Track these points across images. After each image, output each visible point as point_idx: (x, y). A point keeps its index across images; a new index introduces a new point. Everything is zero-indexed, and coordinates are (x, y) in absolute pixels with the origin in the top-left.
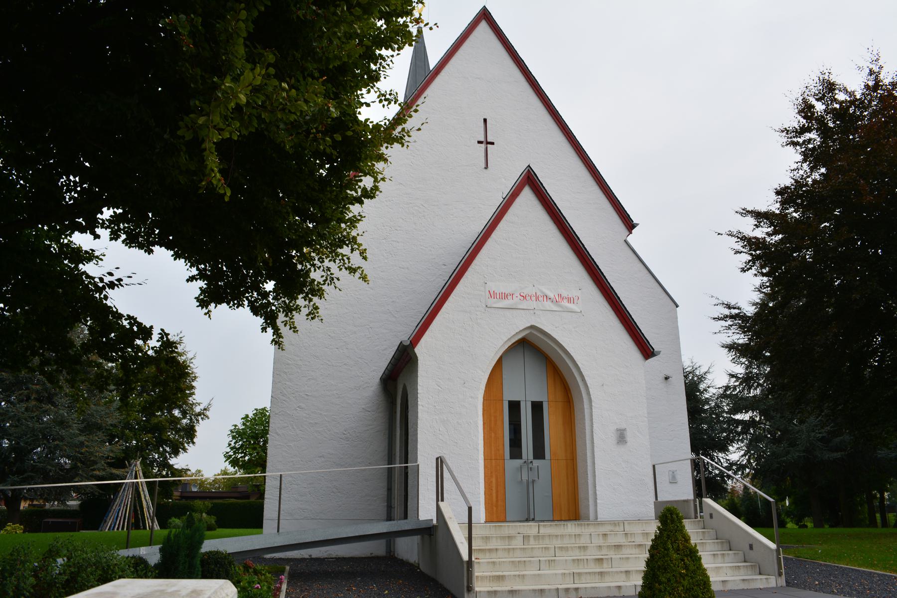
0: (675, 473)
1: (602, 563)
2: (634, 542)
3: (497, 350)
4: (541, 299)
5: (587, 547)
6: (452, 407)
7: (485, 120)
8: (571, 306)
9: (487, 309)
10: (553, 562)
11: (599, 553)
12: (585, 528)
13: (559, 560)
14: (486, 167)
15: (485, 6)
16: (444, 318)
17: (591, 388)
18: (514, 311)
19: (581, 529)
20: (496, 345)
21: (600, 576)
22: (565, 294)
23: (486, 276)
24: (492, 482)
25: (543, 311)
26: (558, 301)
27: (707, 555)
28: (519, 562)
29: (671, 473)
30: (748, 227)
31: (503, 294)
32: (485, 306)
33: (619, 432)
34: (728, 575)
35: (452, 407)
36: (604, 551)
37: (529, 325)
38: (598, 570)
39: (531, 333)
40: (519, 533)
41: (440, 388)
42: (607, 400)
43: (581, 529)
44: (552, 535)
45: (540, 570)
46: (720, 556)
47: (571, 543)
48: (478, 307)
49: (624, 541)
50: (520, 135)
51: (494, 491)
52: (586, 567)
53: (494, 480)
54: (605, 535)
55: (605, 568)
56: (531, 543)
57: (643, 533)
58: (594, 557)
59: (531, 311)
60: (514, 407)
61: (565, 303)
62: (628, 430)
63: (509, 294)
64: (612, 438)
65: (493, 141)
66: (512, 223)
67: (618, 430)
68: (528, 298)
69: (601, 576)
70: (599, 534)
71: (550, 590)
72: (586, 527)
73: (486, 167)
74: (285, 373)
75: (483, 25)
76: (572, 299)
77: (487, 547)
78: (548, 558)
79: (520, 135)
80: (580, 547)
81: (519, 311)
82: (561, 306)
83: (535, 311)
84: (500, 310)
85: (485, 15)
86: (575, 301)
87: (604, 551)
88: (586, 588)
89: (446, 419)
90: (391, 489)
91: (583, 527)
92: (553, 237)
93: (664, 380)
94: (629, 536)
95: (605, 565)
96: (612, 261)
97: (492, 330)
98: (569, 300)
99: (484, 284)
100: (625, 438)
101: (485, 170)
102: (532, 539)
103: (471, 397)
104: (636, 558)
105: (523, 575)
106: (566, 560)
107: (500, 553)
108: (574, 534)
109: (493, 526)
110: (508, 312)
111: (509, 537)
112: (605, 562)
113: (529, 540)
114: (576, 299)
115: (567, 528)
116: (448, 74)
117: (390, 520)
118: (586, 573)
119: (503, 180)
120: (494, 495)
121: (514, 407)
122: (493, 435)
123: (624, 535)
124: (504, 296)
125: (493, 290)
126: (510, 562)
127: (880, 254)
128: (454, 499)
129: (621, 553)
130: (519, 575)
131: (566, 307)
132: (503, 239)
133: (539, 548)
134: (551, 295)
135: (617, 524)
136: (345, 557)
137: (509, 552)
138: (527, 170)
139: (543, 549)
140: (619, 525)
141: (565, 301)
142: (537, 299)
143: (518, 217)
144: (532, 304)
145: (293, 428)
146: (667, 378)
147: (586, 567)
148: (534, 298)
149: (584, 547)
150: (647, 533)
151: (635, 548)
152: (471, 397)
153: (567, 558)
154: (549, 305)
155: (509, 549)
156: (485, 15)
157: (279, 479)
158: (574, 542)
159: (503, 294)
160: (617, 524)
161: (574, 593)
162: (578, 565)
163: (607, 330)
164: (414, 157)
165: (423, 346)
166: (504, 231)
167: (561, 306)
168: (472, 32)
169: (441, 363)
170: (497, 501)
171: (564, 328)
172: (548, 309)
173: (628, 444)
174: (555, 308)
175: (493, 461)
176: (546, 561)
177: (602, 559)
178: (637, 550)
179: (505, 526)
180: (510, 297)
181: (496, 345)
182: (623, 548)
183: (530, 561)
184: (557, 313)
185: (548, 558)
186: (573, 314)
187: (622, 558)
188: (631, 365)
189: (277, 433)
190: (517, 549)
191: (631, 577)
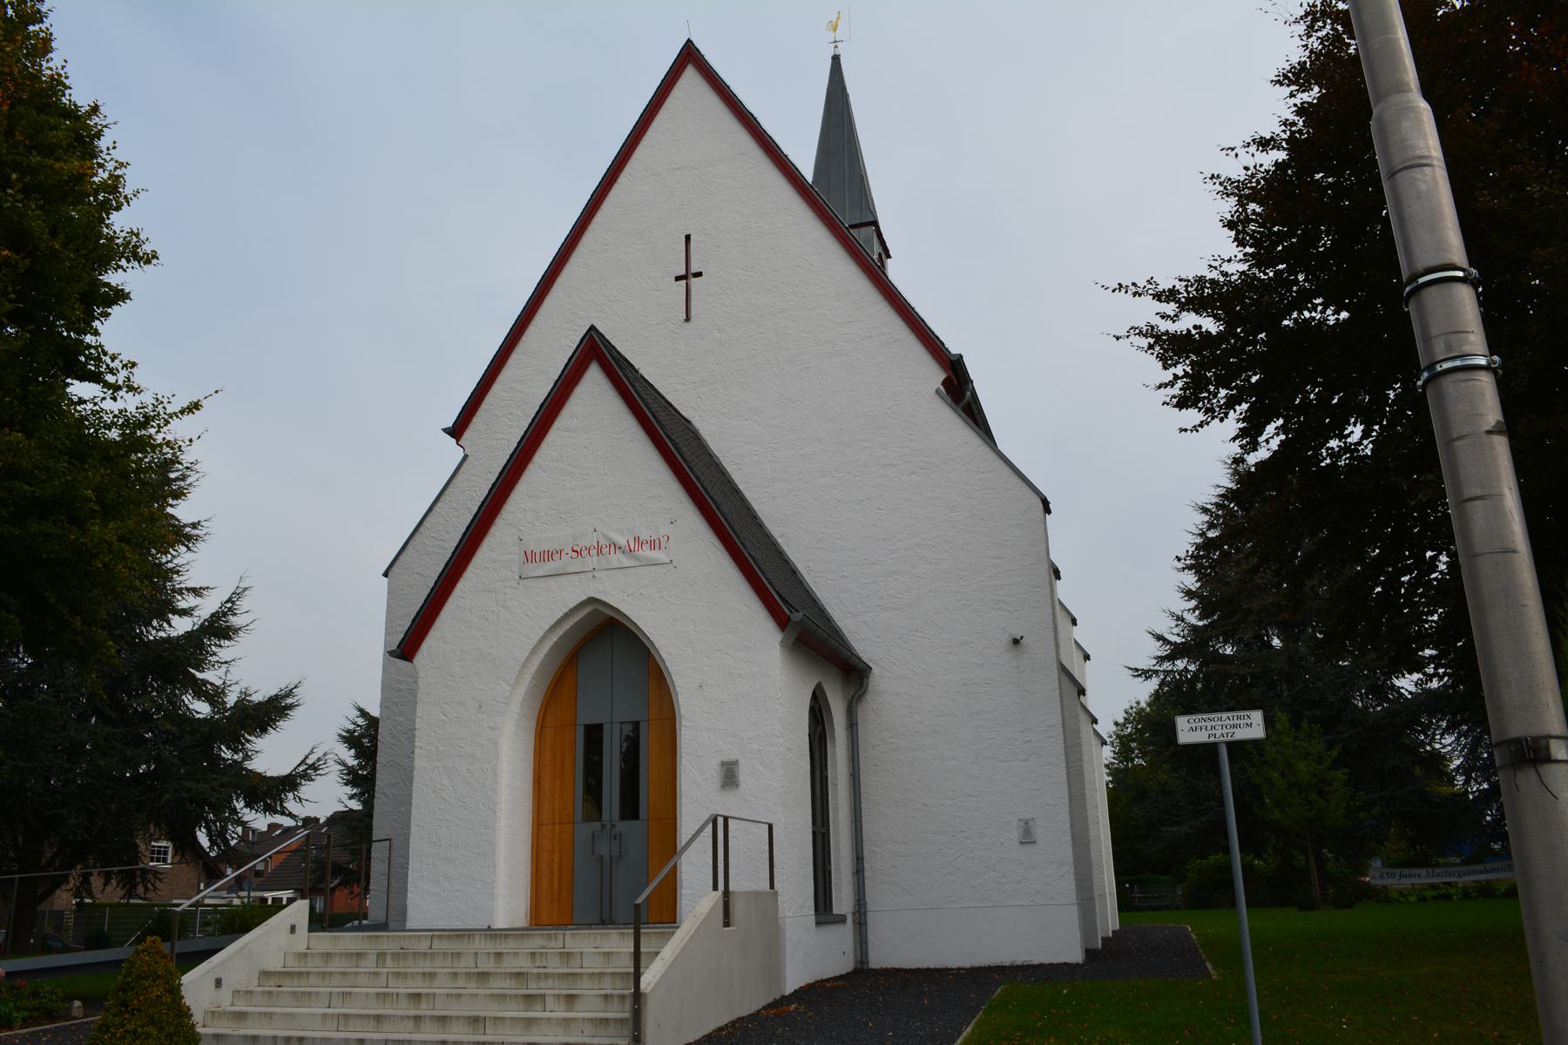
0: (1031, 823)
1: (420, 1002)
2: (544, 967)
3: (531, 647)
4: (605, 550)
5: (435, 973)
6: (462, 747)
7: (688, 238)
8: (657, 555)
9: (522, 582)
10: (348, 996)
11: (453, 985)
12: (469, 942)
13: (357, 993)
14: (688, 319)
15: (689, 40)
16: (458, 606)
17: (681, 694)
18: (563, 579)
19: (495, 943)
20: (531, 639)
21: (375, 1023)
22: (645, 536)
23: (521, 528)
24: (553, 861)
25: (610, 572)
26: (632, 550)
27: (593, 995)
28: (303, 993)
29: (1022, 824)
30: (1148, 312)
31: (546, 553)
32: (517, 577)
33: (725, 767)
34: (586, 1033)
35: (462, 747)
36: (461, 982)
37: (584, 598)
38: (413, 1013)
39: (595, 609)
40: (402, 949)
41: (446, 718)
42: (708, 713)
43: (495, 943)
44: (418, 953)
45: (329, 1007)
46: (616, 1000)
47: (447, 965)
48: (507, 581)
49: (529, 965)
50: (745, 246)
51: (556, 876)
52: (395, 1006)
53: (556, 857)
54: (499, 955)
55: (424, 1010)
56: (387, 966)
57: (561, 953)
58: (446, 991)
59: (590, 574)
60: (594, 735)
61: (646, 552)
63: (555, 552)
64: (714, 776)
65: (700, 270)
66: (568, 431)
67: (723, 764)
68: (585, 553)
69: (378, 1022)
70: (489, 954)
71: (265, 1037)
72: (503, 940)
73: (688, 319)
74: (396, 703)
75: (690, 75)
76: (657, 541)
77: (328, 970)
78: (343, 989)
79: (745, 246)
80: (424, 974)
81: (569, 577)
82: (638, 559)
83: (596, 574)
84: (542, 579)
85: (690, 56)
86: (663, 546)
87: (461, 982)
88: (314, 1038)
89: (451, 765)
90: (858, 859)
91: (498, 941)
92: (632, 440)
93: (1012, 642)
94: (538, 956)
95: (423, 1005)
96: (911, 434)
97: (527, 615)
98: (653, 545)
100: (735, 777)
101: (686, 324)
102: (389, 960)
103: (490, 728)
104: (472, 995)
105: (271, 1014)
106: (367, 994)
107: (313, 980)
108: (451, 951)
109: (367, 936)
110: (551, 581)
111: (357, 954)
112: (424, 999)
113: (385, 961)
115: (473, 941)
116: (630, 177)
117: (1517, 892)
118: (357, 1016)
119: (716, 333)
120: (556, 881)
121: (594, 735)
122: (558, 783)
123: (530, 955)
124: (548, 556)
125: (531, 548)
126: (290, 992)
127: (1344, 315)
128: (457, 890)
129: (488, 986)
130: (265, 1013)
131: (646, 558)
132: (552, 461)
133: (365, 973)
134: (622, 541)
135: (553, 937)
136: (938, 967)
137: (324, 978)
138: (589, 335)
139: (371, 975)
140: (556, 937)
142: (600, 551)
143: (577, 418)
144: (592, 561)
145: (406, 785)
146: (1016, 642)
147: (395, 1006)
148: (594, 552)
149: (430, 974)
150: (568, 953)
151: (511, 979)
152: (490, 728)
153: (369, 990)
154: (617, 559)
155: (324, 973)
156: (690, 56)
157: (387, 861)
158: (450, 965)
159: (546, 553)
160: (553, 937)
161: (297, 1043)
162: (384, 1002)
163: (716, 587)
164: (576, 331)
165: (425, 655)
166: (554, 448)
167: (638, 559)
168: (670, 92)
169: (450, 678)
170: (560, 891)
171: (641, 594)
172: (615, 564)
173: (742, 787)
174: (626, 562)
175: (557, 827)
176: (339, 993)
177: (419, 995)
178: (513, 981)
179: (383, 936)
180: (556, 556)
181: (531, 639)
182: (491, 978)
183: (317, 993)
184: (631, 570)
185: (343, 989)
186: (659, 567)
187: (451, 995)
188: (755, 645)
189: (384, 793)
190: (335, 973)
191: (422, 1025)
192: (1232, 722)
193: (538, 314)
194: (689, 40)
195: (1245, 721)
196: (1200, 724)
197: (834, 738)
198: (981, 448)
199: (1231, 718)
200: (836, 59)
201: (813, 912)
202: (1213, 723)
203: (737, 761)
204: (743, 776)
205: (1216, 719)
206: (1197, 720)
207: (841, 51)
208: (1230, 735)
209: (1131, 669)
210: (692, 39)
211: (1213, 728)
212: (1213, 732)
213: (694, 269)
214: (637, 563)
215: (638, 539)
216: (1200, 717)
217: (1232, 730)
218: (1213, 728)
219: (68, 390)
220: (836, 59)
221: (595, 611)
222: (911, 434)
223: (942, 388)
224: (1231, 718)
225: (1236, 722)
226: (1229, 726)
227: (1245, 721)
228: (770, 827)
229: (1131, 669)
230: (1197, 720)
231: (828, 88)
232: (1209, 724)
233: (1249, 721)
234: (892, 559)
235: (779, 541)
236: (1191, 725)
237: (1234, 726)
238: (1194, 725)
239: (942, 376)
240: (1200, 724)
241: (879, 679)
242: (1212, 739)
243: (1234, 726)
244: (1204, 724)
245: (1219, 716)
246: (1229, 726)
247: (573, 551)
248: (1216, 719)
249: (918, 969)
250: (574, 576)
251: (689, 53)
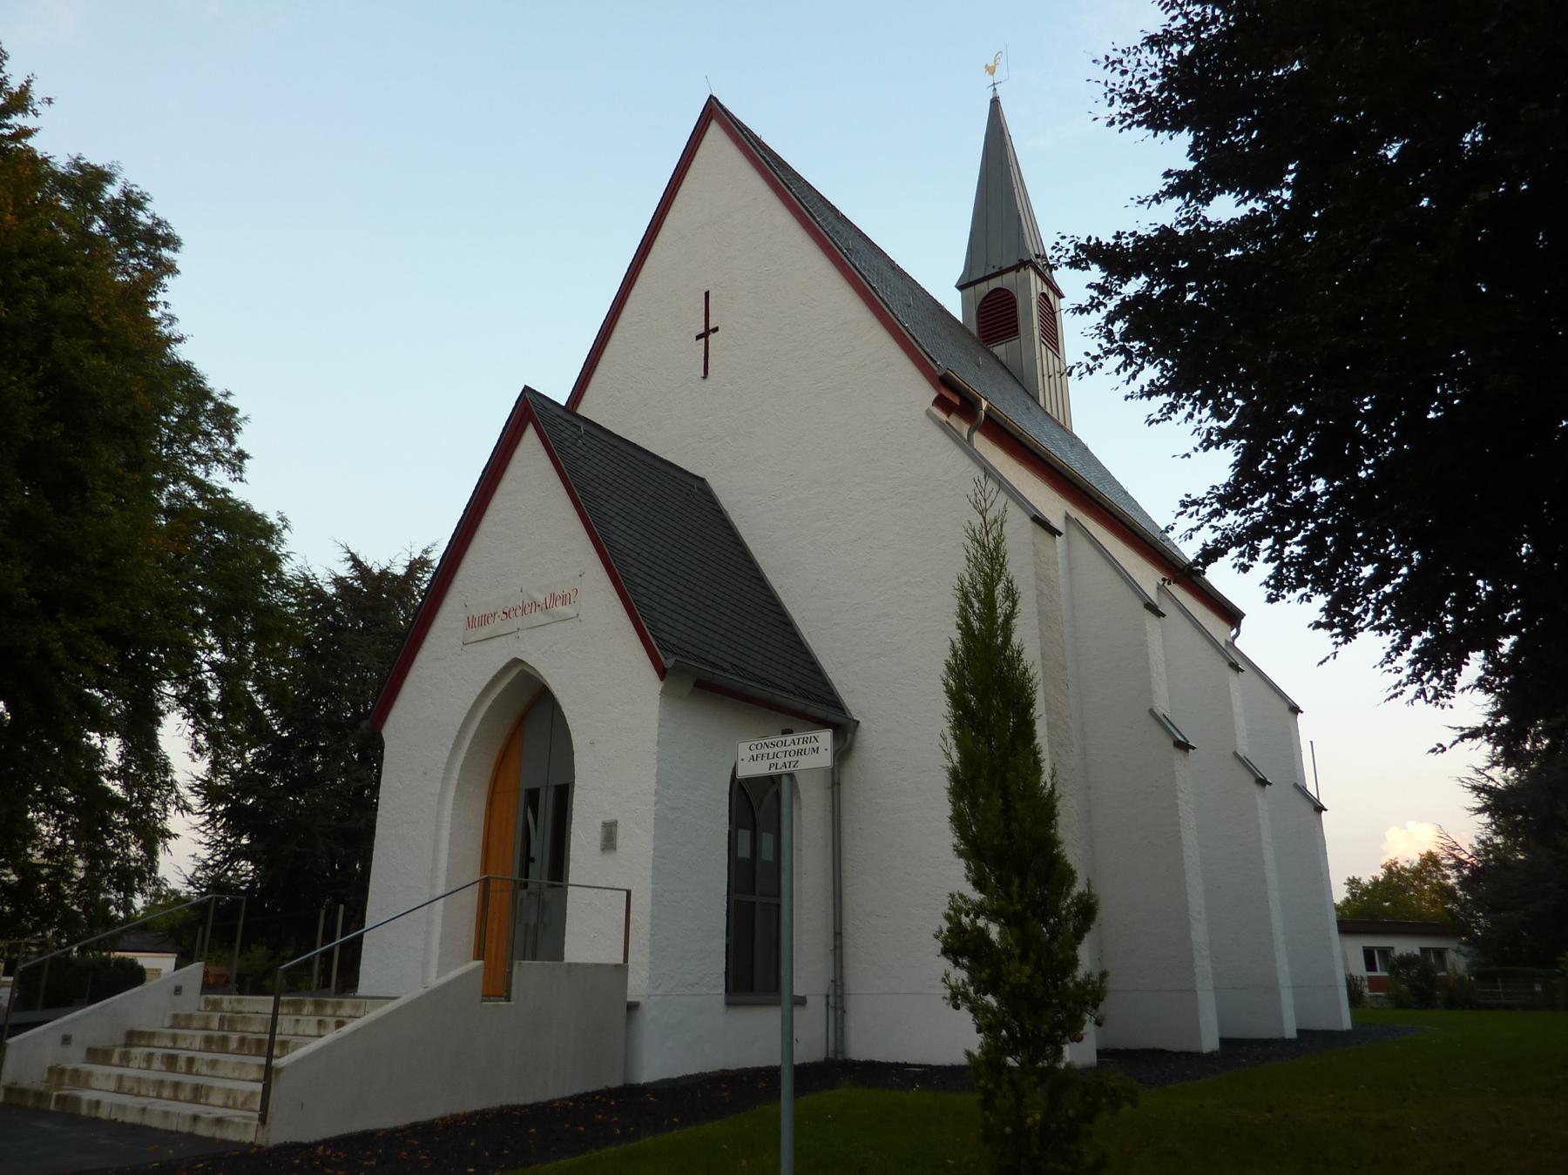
4: (528, 610)
7: (707, 294)
9: (465, 648)
18: (494, 642)
61: (560, 609)
62: (619, 819)
67: (605, 825)
68: (512, 613)
83: (520, 634)
84: (478, 643)
85: (713, 112)
98: (565, 599)
99: (464, 608)
114: (573, 595)
124: (485, 620)
134: (541, 600)
141: (559, 602)
144: (516, 622)
154: (538, 617)
156: (713, 112)
173: (619, 850)
192: (796, 748)
193: (586, 393)
194: (711, 96)
195: (811, 746)
196: (762, 751)
197: (800, 798)
198: (970, 469)
199: (796, 742)
200: (995, 102)
201: (722, 990)
202: (776, 749)
203: (616, 821)
204: (621, 839)
205: (780, 744)
206: (759, 746)
207: (999, 93)
208: (792, 764)
209: (1455, 728)
210: (714, 95)
211: (776, 755)
212: (775, 760)
213: (711, 327)
214: (551, 620)
215: (552, 595)
216: (763, 742)
217: (795, 758)
218: (776, 755)
219: (1321, 600)
220: (995, 102)
221: (523, 671)
222: (901, 463)
223: (937, 411)
224: (796, 742)
225: (801, 746)
226: (792, 753)
227: (811, 746)
228: (629, 893)
229: (1455, 728)
230: (759, 746)
231: (987, 133)
232: (771, 751)
233: (815, 745)
234: (881, 601)
235: (779, 592)
236: (752, 753)
237: (798, 753)
238: (755, 753)
239: (933, 395)
240: (762, 751)
241: (1172, 747)
242: (773, 770)
243: (798, 753)
244: (766, 750)
245: (783, 739)
246: (792, 753)
247: (504, 613)
248: (780, 744)
249: (897, 1063)
250: (504, 638)
251: (711, 109)
